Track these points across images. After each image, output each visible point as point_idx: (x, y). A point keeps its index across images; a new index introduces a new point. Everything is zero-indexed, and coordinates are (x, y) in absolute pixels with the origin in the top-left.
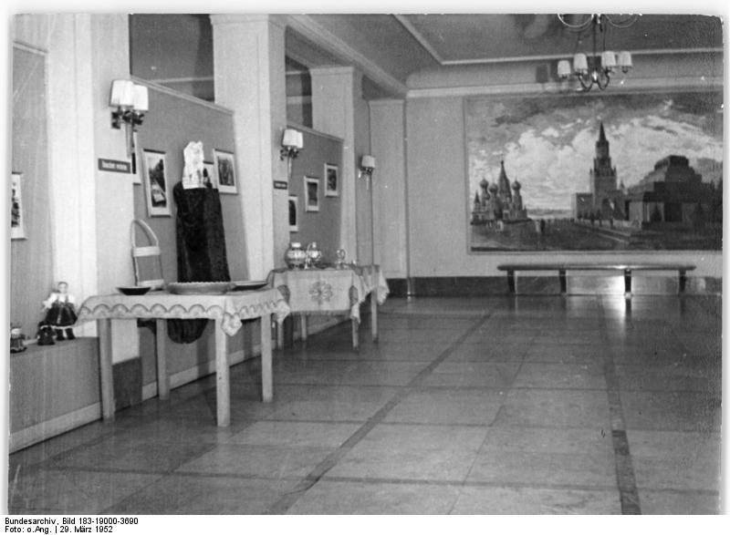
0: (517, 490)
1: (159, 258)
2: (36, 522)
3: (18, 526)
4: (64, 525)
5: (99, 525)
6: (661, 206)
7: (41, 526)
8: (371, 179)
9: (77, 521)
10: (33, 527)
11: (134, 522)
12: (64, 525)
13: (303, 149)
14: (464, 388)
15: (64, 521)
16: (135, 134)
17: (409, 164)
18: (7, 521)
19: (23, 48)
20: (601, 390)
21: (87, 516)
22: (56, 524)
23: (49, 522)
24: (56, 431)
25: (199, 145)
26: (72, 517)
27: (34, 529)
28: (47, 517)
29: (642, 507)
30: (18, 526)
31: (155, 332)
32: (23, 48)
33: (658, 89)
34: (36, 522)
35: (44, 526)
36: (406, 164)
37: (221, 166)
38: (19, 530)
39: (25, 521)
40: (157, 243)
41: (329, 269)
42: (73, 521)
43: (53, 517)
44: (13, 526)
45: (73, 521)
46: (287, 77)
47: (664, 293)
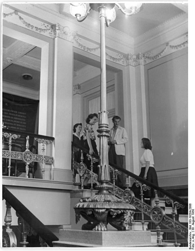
0: (111, 142)
2: (191, 239)
3: (192, 245)
4: (192, 229)
5: (192, 214)
7: (192, 237)
8: (171, 41)
9: (190, 224)
10: (192, 240)
12: (192, 229)
14: (50, 173)
15: (190, 229)
17: (152, 67)
18: (190, 249)
22: (191, 232)
23: (191, 234)
24: (114, 17)
26: (189, 226)
28: (189, 235)
29: (73, 199)
30: (192, 245)
34: (191, 239)
35: (192, 236)
36: (152, 68)
38: (193, 244)
39: (190, 242)
43: (189, 233)
44: (192, 247)
45: (190, 226)
46: (3, 177)
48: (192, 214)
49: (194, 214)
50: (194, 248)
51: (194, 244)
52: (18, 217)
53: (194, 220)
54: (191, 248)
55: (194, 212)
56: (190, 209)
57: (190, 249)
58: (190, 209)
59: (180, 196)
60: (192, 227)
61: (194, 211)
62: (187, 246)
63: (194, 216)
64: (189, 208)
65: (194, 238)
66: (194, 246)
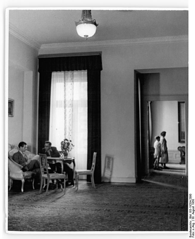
1: (182, 139)
2: (191, 227)
3: (192, 233)
4: (192, 218)
5: (192, 204)
7: (192, 226)
9: (191, 214)
10: (192, 228)
11: (191, 195)
12: (192, 218)
13: (77, 24)
15: (190, 218)
16: (160, 158)
18: (190, 237)
20: (99, 221)
22: (191, 221)
23: (191, 223)
30: (192, 233)
31: (180, 163)
34: (191, 227)
35: (192, 225)
37: (111, 166)
38: (193, 233)
39: (191, 231)
41: (95, 26)
42: (191, 215)
44: (192, 235)
45: (191, 215)
48: (192, 204)
49: (194, 204)
50: (194, 236)
51: (194, 232)
52: (52, 146)
53: (194, 210)
54: (192, 236)
55: (194, 202)
56: (190, 199)
57: (190, 237)
58: (190, 199)
59: (140, 79)
61: (194, 201)
63: (194, 205)
64: (189, 198)
65: (194, 227)
66: (194, 235)
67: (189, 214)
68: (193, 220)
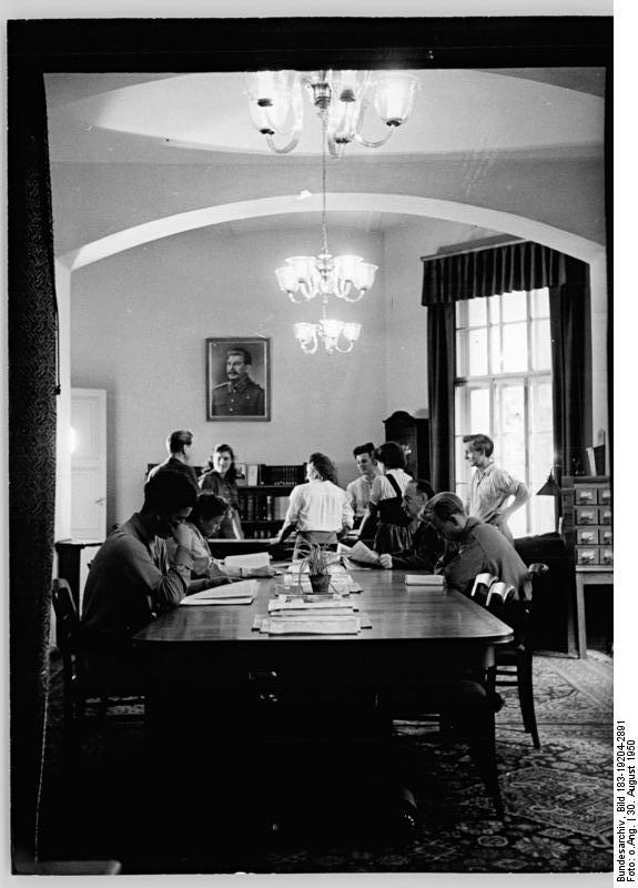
2: (622, 845)
3: (627, 867)
6: (229, 353)
7: (627, 839)
9: (621, 794)
10: (628, 847)
15: (621, 810)
18: (620, 879)
19: (434, 274)
21: (615, 782)
23: (623, 829)
25: (237, 481)
26: (616, 801)
27: (631, 847)
30: (627, 867)
32: (434, 274)
33: (498, 541)
34: (622, 845)
35: (627, 834)
38: (632, 864)
39: (622, 857)
40: (347, 299)
43: (616, 824)
44: (627, 872)
45: (622, 799)
47: (297, 325)
50: (635, 878)
55: (636, 751)
56: (621, 741)
58: (621, 741)
60: (627, 803)
61: (636, 867)
62: (611, 869)
63: (634, 763)
64: (615, 736)
65: (636, 842)
67: (617, 794)
68: (631, 816)
